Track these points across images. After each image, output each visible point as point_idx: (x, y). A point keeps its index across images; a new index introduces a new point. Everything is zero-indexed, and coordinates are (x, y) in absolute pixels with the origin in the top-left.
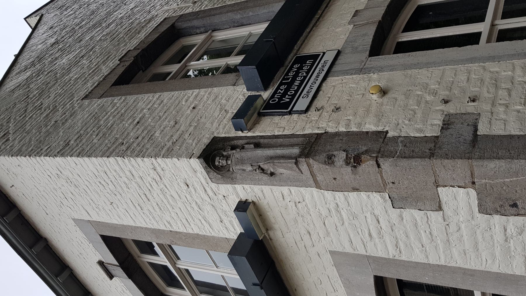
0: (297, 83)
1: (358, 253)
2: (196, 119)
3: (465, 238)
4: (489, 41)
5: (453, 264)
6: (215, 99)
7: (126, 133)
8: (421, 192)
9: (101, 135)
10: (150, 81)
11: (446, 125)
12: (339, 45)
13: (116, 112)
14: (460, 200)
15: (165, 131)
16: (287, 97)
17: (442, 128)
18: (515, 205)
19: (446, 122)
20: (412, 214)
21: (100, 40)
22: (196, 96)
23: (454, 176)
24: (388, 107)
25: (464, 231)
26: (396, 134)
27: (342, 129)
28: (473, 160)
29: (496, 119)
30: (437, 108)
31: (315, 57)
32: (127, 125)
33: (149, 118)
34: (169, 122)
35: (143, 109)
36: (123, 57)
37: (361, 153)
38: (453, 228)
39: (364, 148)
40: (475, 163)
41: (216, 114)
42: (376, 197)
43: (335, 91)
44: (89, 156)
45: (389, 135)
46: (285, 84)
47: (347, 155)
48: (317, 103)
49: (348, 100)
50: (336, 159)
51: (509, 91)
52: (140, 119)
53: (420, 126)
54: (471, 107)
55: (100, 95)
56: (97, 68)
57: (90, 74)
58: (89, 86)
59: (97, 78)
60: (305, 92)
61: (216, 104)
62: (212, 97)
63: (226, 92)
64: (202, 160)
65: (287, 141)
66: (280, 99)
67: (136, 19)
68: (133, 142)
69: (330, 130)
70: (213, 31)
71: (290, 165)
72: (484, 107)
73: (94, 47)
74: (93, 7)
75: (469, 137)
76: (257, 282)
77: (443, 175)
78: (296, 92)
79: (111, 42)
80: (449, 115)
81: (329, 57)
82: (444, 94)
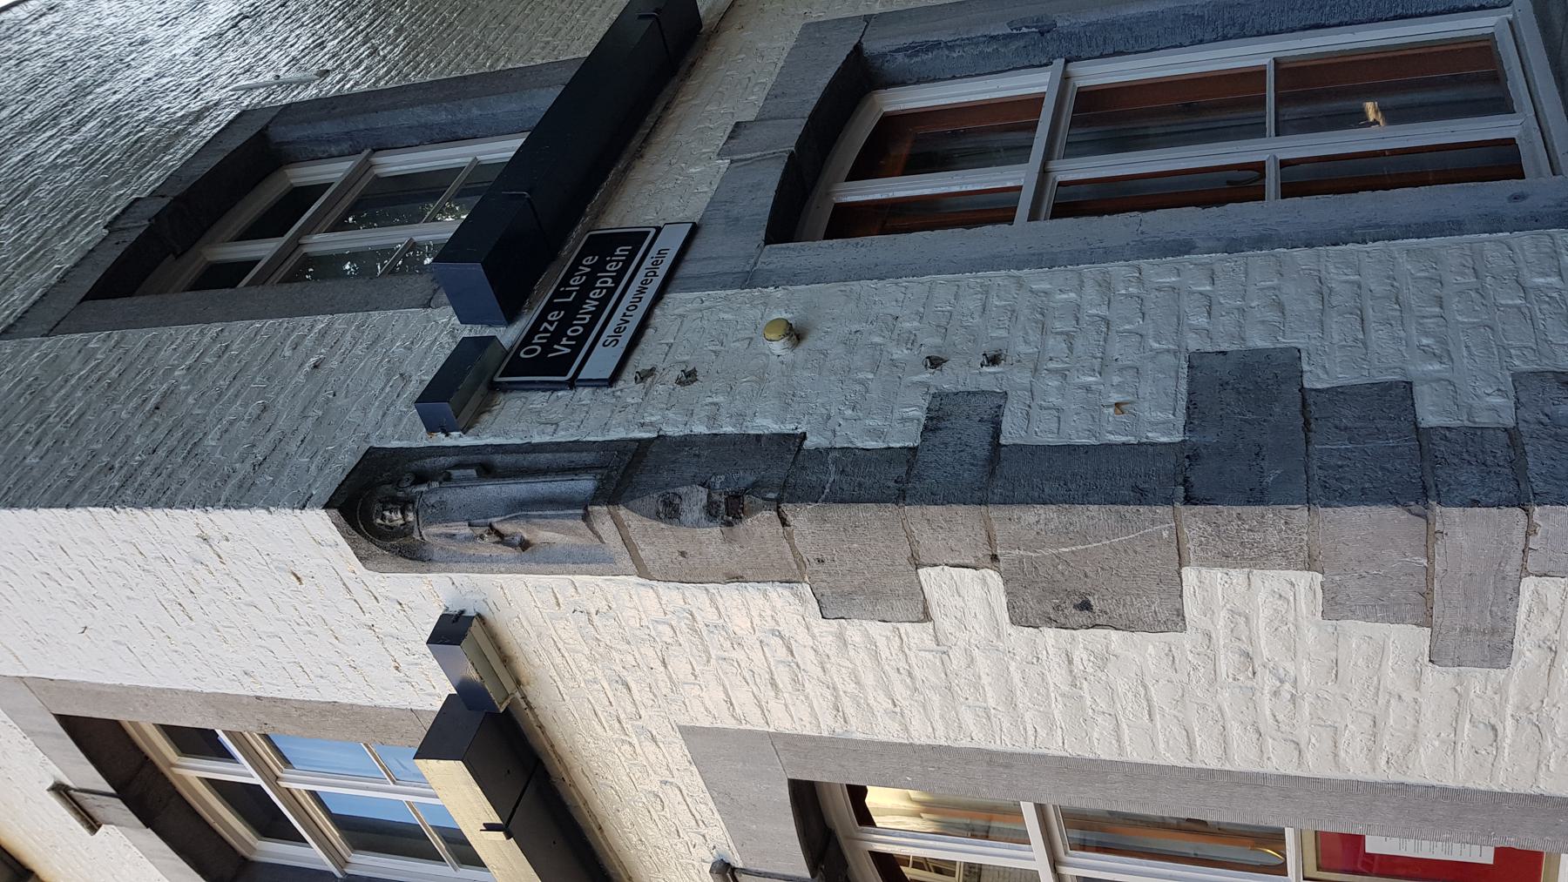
0: (590, 306)
1: (749, 727)
2: (320, 399)
3: (985, 680)
4: (1033, 216)
5: (965, 743)
6: (374, 342)
7: (122, 437)
8: (884, 581)
9: (48, 442)
10: (197, 286)
11: (932, 425)
12: (694, 209)
13: (95, 377)
14: (966, 595)
15: (233, 431)
16: (564, 341)
17: (925, 427)
18: (1085, 606)
19: (933, 414)
20: (864, 631)
21: (54, 166)
22: (323, 334)
23: (952, 543)
24: (806, 374)
25: (983, 664)
26: (825, 443)
27: (700, 429)
28: (991, 508)
29: (1041, 407)
30: (916, 378)
31: (635, 239)
32: (124, 415)
33: (189, 393)
34: (245, 405)
35: (174, 368)
36: (117, 217)
37: (736, 486)
38: (957, 661)
39: (751, 479)
40: (995, 512)
41: (377, 385)
42: (779, 596)
43: (684, 329)
44: (12, 506)
45: (808, 444)
46: (559, 307)
47: (709, 496)
48: (640, 361)
49: (723, 351)
50: (684, 506)
51: (1069, 337)
52: (164, 396)
53: (874, 422)
54: (988, 379)
55: (47, 327)
56: (40, 248)
57: (19, 265)
58: (18, 299)
59: (41, 278)
60: (609, 330)
61: (382, 357)
62: (367, 337)
63: (406, 325)
64: (335, 512)
65: (563, 458)
66: (547, 348)
67: (159, 110)
68: (142, 463)
69: (671, 431)
70: (375, 151)
71: (570, 523)
72: (1012, 377)
73: (34, 186)
74: (36, 67)
75: (982, 452)
76: (497, 820)
77: (927, 539)
78: (588, 328)
79: (83, 172)
80: (939, 396)
81: (671, 242)
82: (931, 343)
